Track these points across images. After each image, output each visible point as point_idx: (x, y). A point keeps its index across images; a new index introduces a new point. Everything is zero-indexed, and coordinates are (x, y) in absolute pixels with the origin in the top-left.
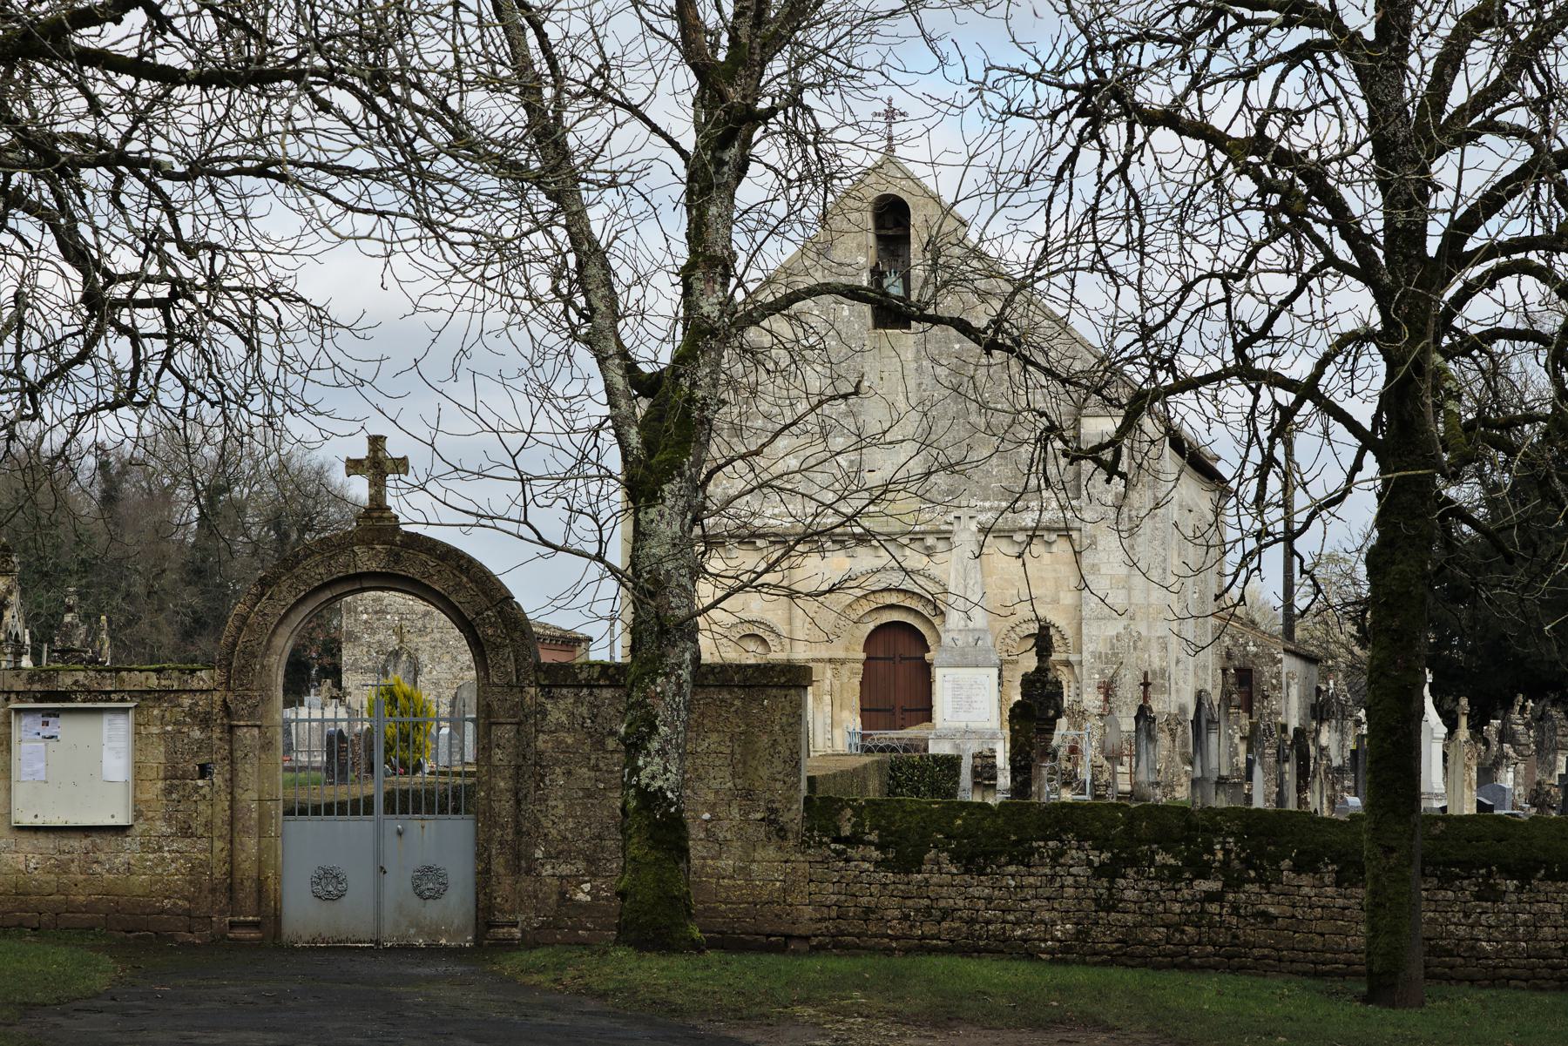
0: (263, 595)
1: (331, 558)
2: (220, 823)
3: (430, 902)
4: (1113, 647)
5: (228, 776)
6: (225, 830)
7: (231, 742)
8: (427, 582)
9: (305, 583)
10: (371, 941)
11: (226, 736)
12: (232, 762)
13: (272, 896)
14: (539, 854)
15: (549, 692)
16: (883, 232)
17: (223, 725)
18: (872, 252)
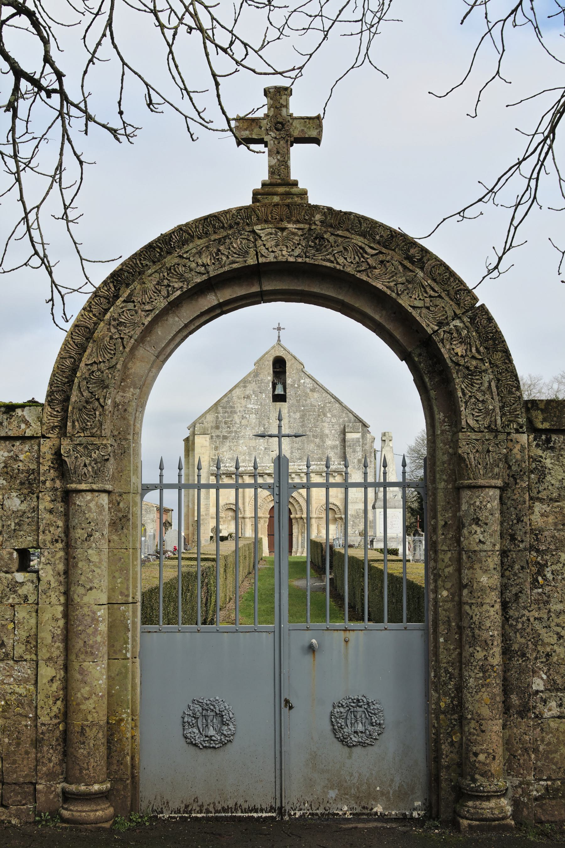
0: (117, 297)
1: (220, 241)
2: (49, 640)
3: (358, 750)
4: (357, 513)
5: (61, 567)
6: (57, 649)
7: (66, 516)
8: (364, 278)
9: (181, 278)
10: (272, 809)
11: (60, 507)
12: (68, 547)
13: (128, 749)
14: (538, 684)
15: (548, 441)
16: (275, 370)
17: (55, 489)
18: (272, 376)
